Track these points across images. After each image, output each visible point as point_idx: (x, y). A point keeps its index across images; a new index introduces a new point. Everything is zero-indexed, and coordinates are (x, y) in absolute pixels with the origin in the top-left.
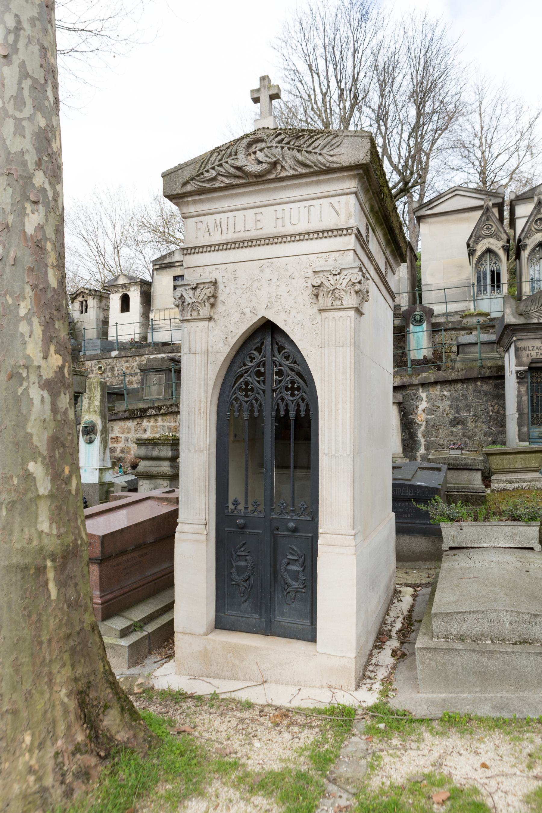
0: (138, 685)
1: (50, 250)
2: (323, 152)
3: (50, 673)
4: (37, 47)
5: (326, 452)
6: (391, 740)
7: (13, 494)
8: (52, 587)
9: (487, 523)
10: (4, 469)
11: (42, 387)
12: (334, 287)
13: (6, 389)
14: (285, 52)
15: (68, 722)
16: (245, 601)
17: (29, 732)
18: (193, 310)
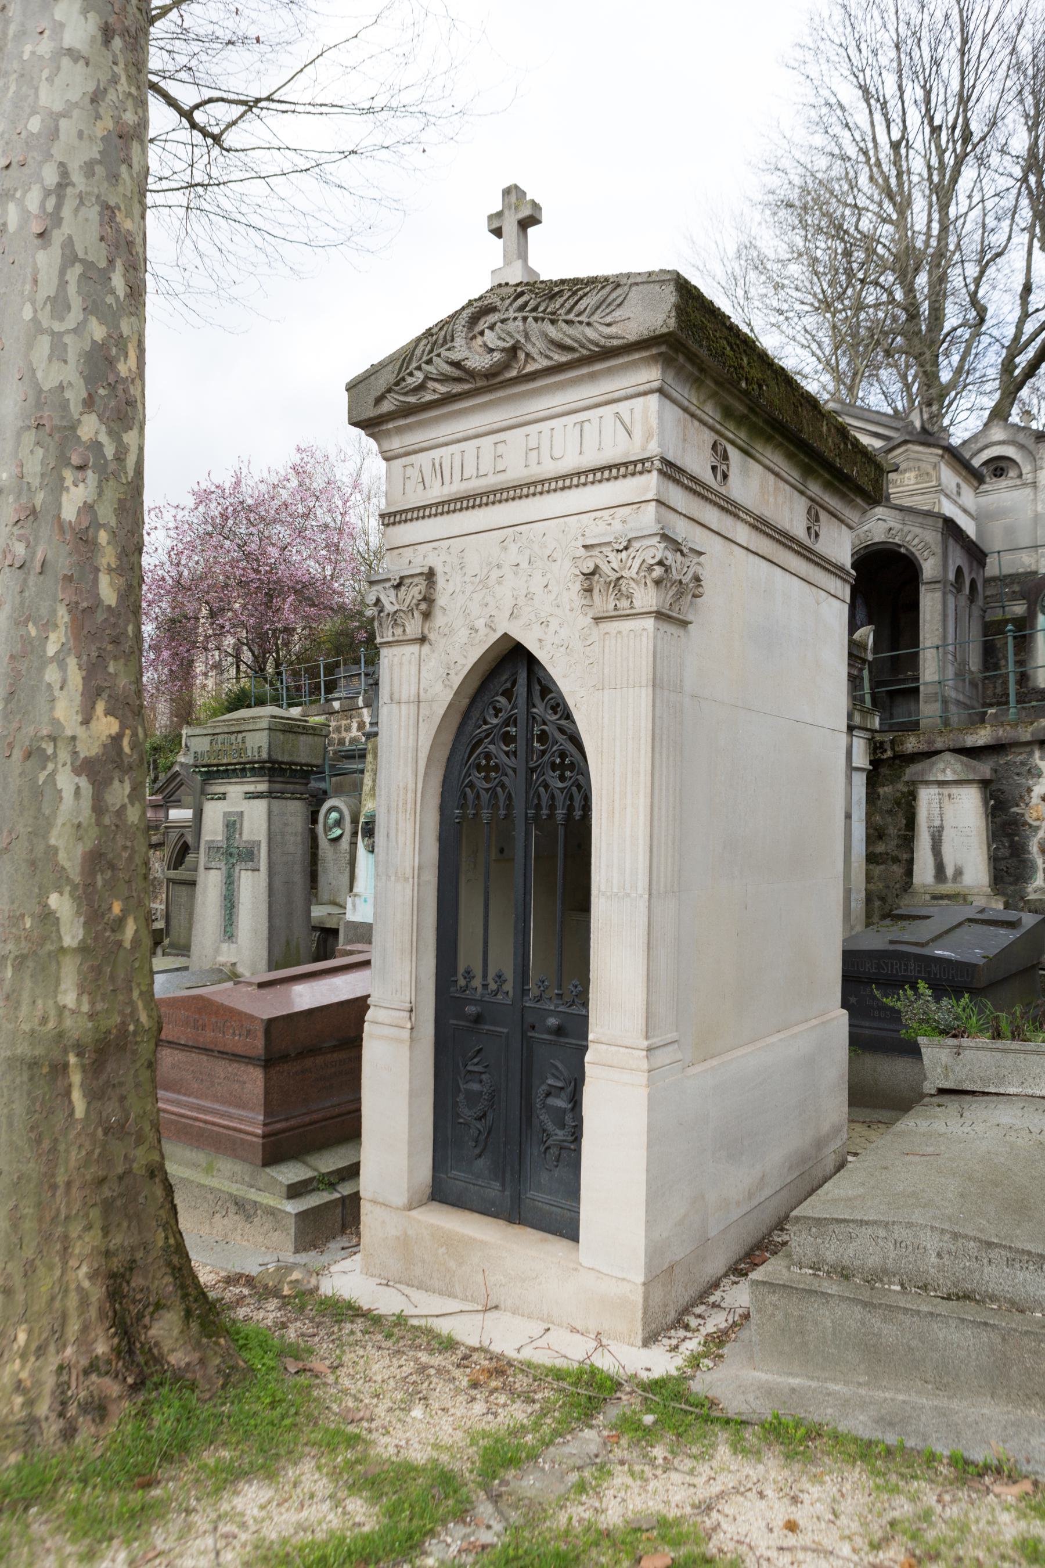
0: (291, 1282)
1: (104, 543)
2: (596, 317)
3: (66, 1237)
4: (97, 208)
5: (603, 888)
6: (652, 1446)
7: (23, 944)
8: (77, 1097)
9: (1016, 1045)
10: (13, 903)
11: (77, 771)
12: (618, 575)
13: (20, 775)
14: (813, 70)
15: (85, 1320)
16: (480, 1156)
17: (24, 1326)
18: (396, 624)
